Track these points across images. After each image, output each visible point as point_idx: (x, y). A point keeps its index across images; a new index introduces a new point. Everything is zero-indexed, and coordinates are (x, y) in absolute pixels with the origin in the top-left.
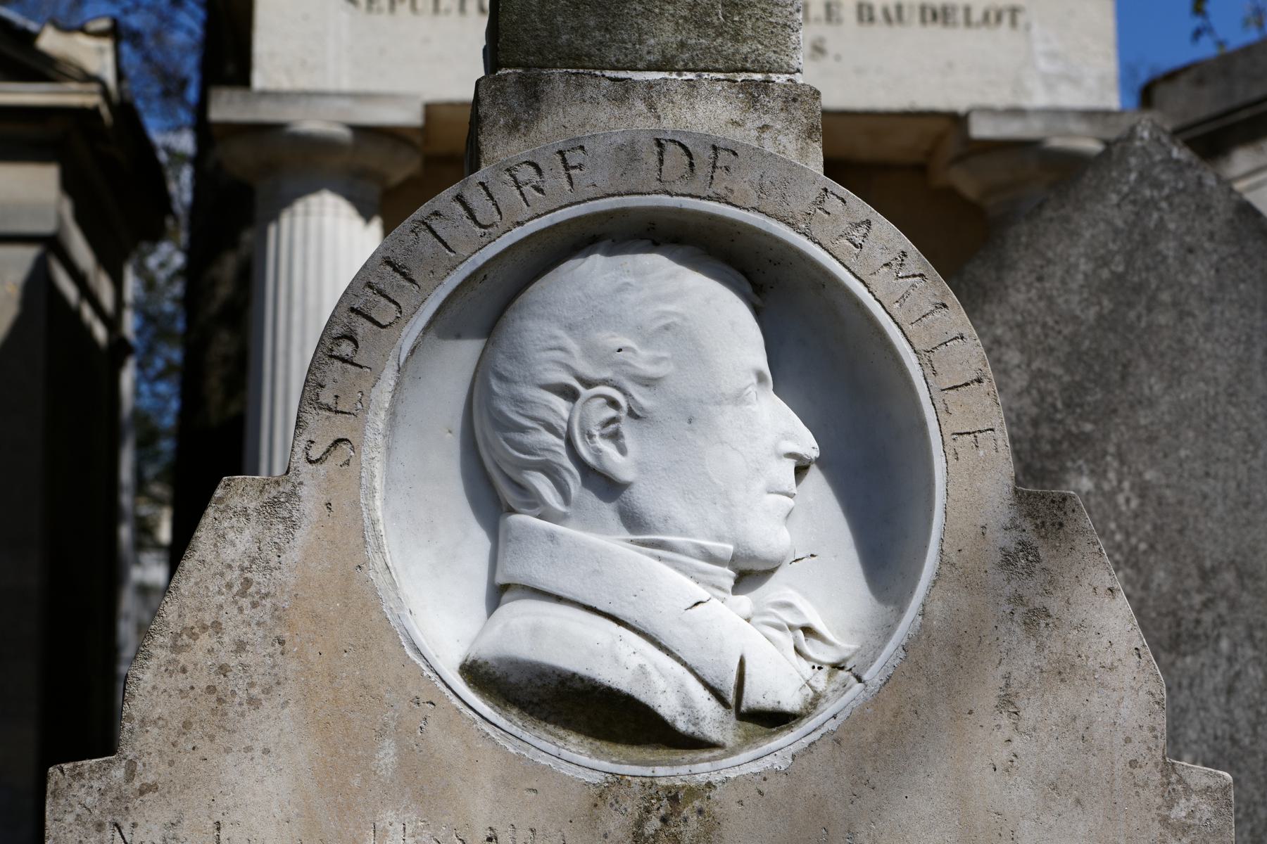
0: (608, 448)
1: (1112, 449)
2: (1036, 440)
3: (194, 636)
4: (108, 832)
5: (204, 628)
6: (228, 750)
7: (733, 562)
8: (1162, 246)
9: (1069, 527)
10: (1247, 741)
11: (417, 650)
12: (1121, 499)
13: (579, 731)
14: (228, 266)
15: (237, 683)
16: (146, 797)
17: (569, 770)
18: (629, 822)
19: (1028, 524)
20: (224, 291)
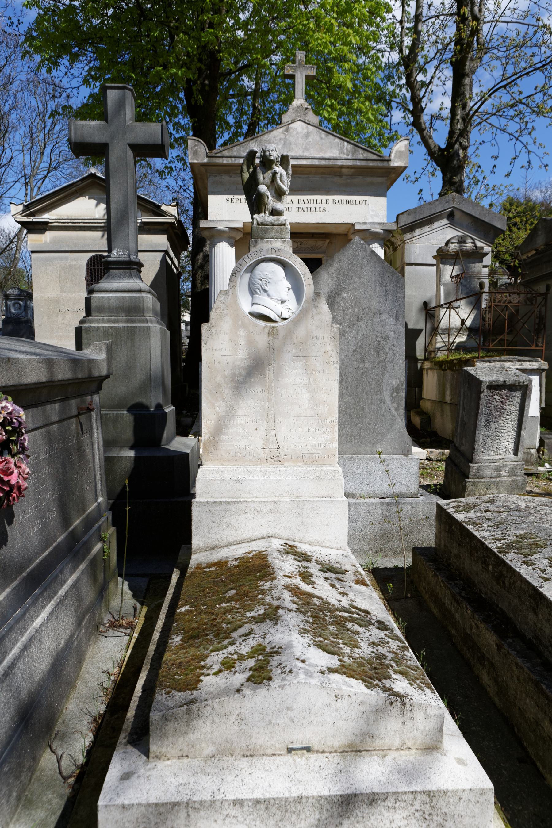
14: (200, 256)
15: (223, 314)
20: (200, 261)
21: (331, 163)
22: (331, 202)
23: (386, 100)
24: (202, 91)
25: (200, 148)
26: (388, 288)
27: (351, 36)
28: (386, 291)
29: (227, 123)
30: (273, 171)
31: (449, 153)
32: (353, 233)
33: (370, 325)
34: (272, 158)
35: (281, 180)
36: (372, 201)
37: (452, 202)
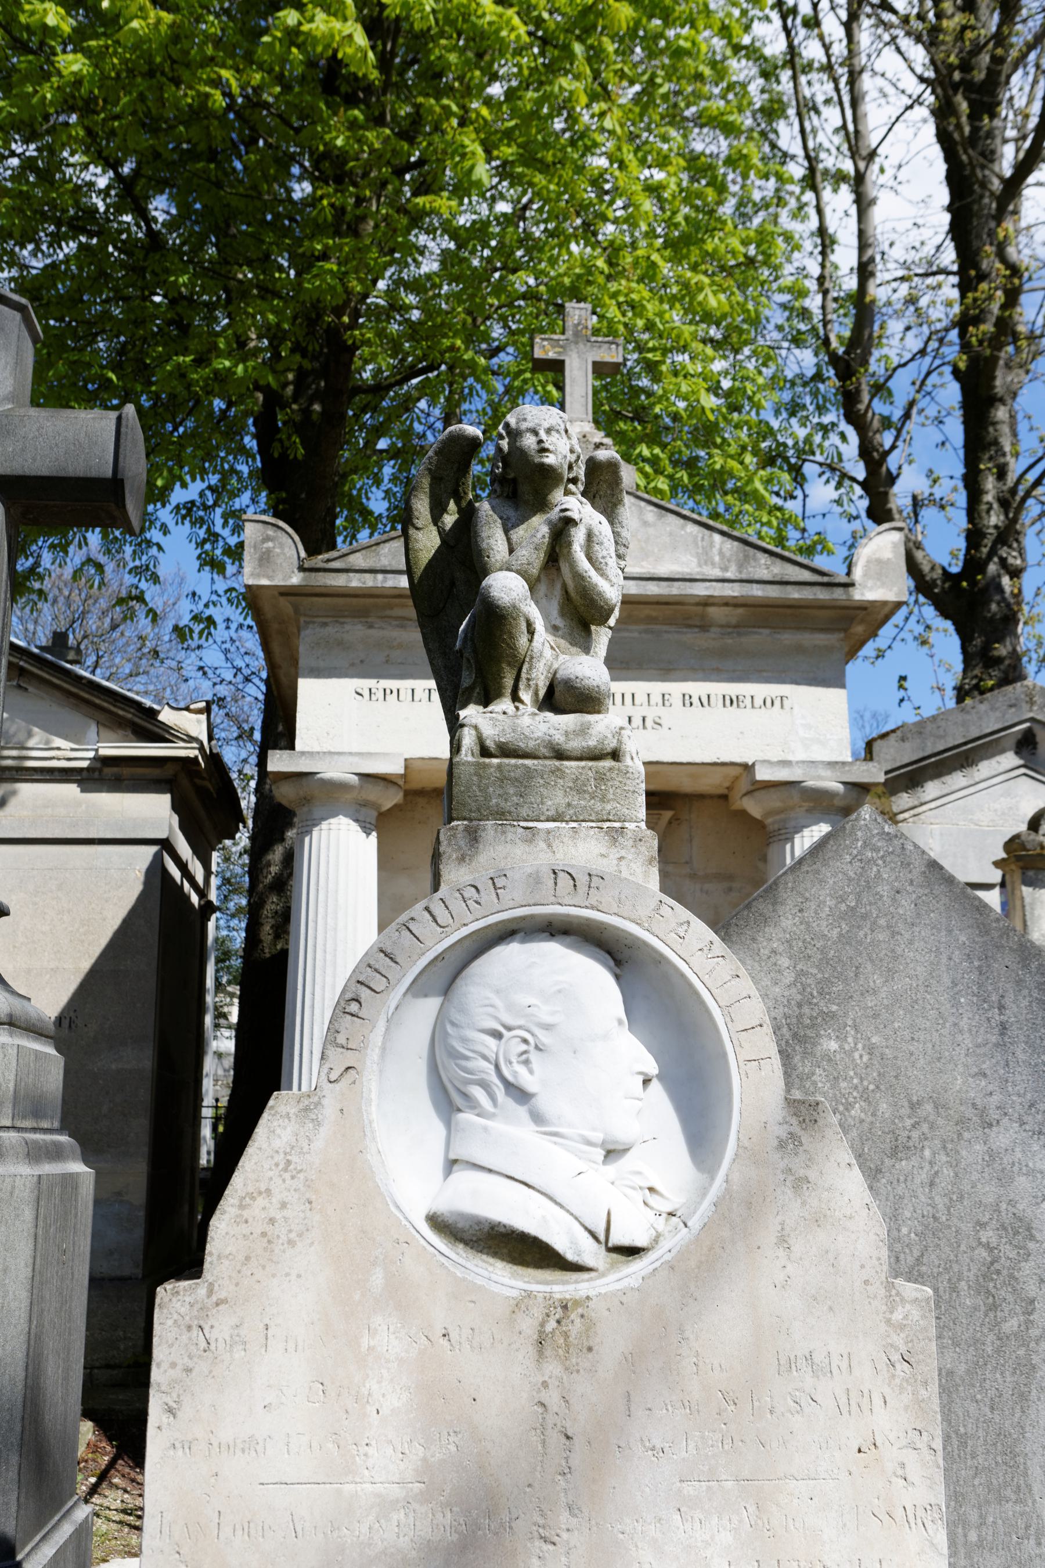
0: (521, 1070)
1: (850, 1023)
2: (800, 1016)
3: (253, 1199)
4: (195, 1331)
5: (260, 1193)
6: (274, 1276)
7: (603, 1144)
8: (879, 889)
9: (820, 1123)
10: (944, 1218)
11: (398, 1207)
12: (856, 1055)
13: (477, 535)
14: (277, 855)
16: (220, 1308)
17: (496, 1288)
18: (536, 1323)
19: (794, 1121)
20: (274, 869)
22: (677, 700)
24: (304, 426)
26: (1009, 1016)
27: (708, 290)
28: (1003, 1027)
29: (366, 513)
30: (554, 514)
31: (973, 583)
32: (749, 793)
33: (948, 1172)
34: (550, 460)
35: (589, 558)
36: (805, 699)
37: (1025, 707)
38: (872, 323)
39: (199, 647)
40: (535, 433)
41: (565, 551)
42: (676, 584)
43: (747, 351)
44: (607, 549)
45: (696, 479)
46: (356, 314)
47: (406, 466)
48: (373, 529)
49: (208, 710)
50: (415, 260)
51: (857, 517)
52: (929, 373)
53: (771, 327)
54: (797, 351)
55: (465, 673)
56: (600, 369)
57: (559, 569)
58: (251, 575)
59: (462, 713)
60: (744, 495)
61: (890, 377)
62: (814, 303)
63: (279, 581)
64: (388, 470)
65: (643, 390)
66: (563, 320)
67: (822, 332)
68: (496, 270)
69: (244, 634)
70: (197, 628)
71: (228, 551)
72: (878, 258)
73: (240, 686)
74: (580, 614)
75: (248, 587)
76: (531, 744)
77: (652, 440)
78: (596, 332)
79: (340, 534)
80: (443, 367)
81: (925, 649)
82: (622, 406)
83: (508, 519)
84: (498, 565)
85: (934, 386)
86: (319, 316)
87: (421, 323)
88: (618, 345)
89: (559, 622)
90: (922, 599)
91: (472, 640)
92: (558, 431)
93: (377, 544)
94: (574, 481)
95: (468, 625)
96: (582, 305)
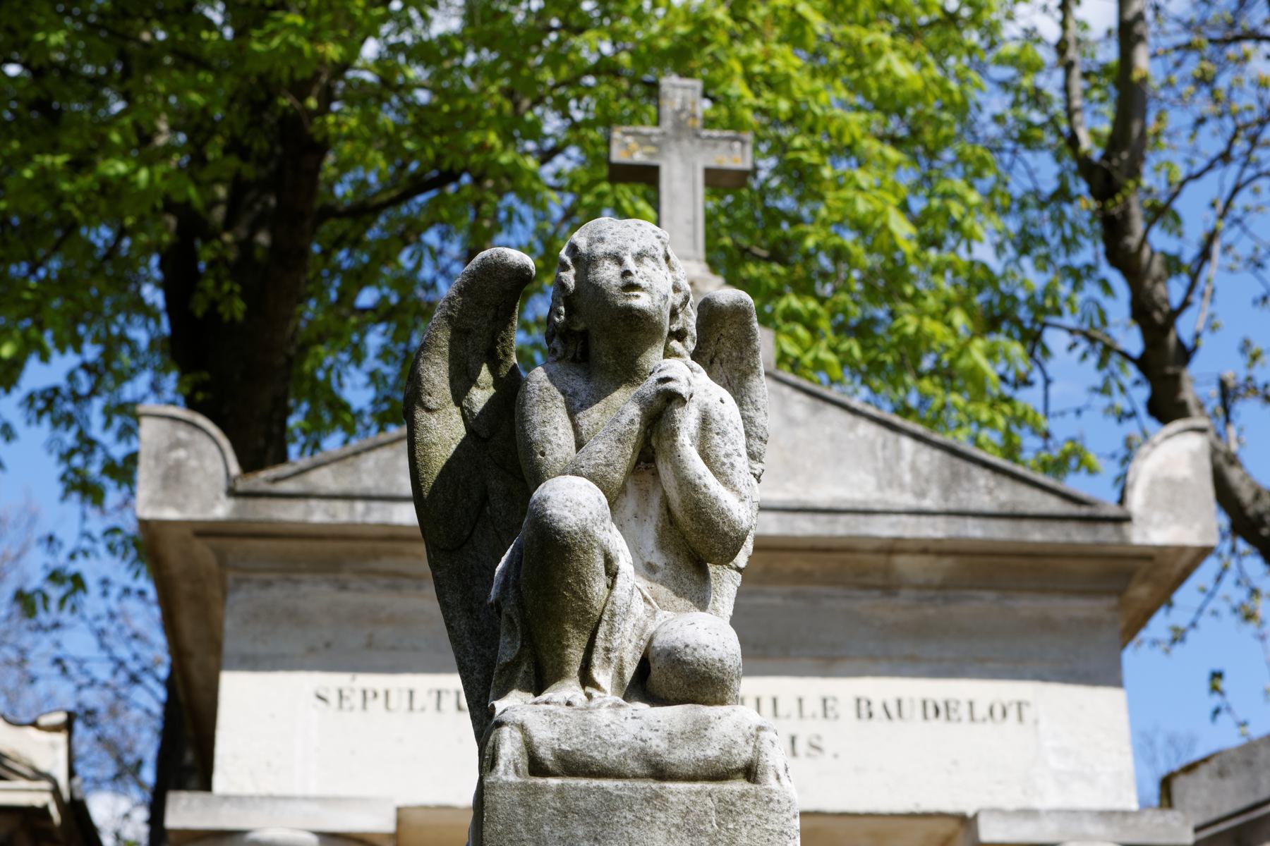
13: (524, 419)
21: (841, 528)
22: (846, 709)
23: (1018, 323)
25: (200, 455)
29: (339, 407)
30: (648, 386)
34: (642, 301)
38: (1143, 114)
39: (57, 626)
40: (618, 260)
41: (666, 444)
42: (843, 519)
43: (948, 155)
44: (732, 443)
45: (873, 353)
46: (327, 97)
47: (402, 334)
48: (350, 430)
49: (67, 727)
50: (423, 16)
51: (1132, 415)
52: (1236, 190)
53: (985, 117)
54: (1027, 156)
55: (504, 640)
56: (716, 180)
57: (656, 474)
58: (150, 502)
59: (500, 705)
60: (947, 376)
61: (1175, 195)
62: (1051, 83)
63: (194, 513)
64: (375, 339)
65: (783, 215)
66: (658, 107)
67: (1064, 127)
68: (551, 29)
69: (132, 604)
70: (55, 593)
71: (111, 469)
72: (1149, 15)
73: (123, 691)
74: (692, 546)
75: (144, 524)
76: (613, 754)
77: (804, 288)
78: (709, 123)
79: (294, 440)
80: (466, 179)
81: (1251, 627)
82: (748, 232)
83: (575, 394)
84: (558, 467)
85: (1246, 210)
86: (271, 97)
87: (430, 108)
88: (743, 142)
89: (657, 559)
90: (1242, 546)
91: (516, 586)
92: (653, 258)
93: (356, 454)
94: (680, 335)
95: (509, 562)
96: (687, 82)
